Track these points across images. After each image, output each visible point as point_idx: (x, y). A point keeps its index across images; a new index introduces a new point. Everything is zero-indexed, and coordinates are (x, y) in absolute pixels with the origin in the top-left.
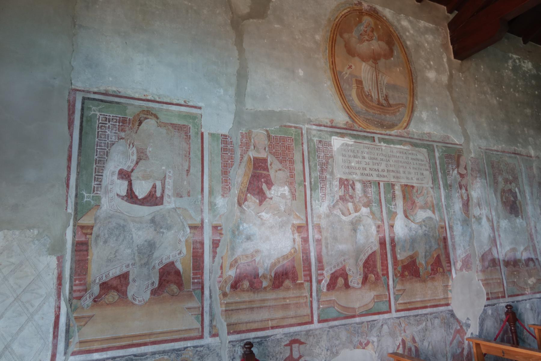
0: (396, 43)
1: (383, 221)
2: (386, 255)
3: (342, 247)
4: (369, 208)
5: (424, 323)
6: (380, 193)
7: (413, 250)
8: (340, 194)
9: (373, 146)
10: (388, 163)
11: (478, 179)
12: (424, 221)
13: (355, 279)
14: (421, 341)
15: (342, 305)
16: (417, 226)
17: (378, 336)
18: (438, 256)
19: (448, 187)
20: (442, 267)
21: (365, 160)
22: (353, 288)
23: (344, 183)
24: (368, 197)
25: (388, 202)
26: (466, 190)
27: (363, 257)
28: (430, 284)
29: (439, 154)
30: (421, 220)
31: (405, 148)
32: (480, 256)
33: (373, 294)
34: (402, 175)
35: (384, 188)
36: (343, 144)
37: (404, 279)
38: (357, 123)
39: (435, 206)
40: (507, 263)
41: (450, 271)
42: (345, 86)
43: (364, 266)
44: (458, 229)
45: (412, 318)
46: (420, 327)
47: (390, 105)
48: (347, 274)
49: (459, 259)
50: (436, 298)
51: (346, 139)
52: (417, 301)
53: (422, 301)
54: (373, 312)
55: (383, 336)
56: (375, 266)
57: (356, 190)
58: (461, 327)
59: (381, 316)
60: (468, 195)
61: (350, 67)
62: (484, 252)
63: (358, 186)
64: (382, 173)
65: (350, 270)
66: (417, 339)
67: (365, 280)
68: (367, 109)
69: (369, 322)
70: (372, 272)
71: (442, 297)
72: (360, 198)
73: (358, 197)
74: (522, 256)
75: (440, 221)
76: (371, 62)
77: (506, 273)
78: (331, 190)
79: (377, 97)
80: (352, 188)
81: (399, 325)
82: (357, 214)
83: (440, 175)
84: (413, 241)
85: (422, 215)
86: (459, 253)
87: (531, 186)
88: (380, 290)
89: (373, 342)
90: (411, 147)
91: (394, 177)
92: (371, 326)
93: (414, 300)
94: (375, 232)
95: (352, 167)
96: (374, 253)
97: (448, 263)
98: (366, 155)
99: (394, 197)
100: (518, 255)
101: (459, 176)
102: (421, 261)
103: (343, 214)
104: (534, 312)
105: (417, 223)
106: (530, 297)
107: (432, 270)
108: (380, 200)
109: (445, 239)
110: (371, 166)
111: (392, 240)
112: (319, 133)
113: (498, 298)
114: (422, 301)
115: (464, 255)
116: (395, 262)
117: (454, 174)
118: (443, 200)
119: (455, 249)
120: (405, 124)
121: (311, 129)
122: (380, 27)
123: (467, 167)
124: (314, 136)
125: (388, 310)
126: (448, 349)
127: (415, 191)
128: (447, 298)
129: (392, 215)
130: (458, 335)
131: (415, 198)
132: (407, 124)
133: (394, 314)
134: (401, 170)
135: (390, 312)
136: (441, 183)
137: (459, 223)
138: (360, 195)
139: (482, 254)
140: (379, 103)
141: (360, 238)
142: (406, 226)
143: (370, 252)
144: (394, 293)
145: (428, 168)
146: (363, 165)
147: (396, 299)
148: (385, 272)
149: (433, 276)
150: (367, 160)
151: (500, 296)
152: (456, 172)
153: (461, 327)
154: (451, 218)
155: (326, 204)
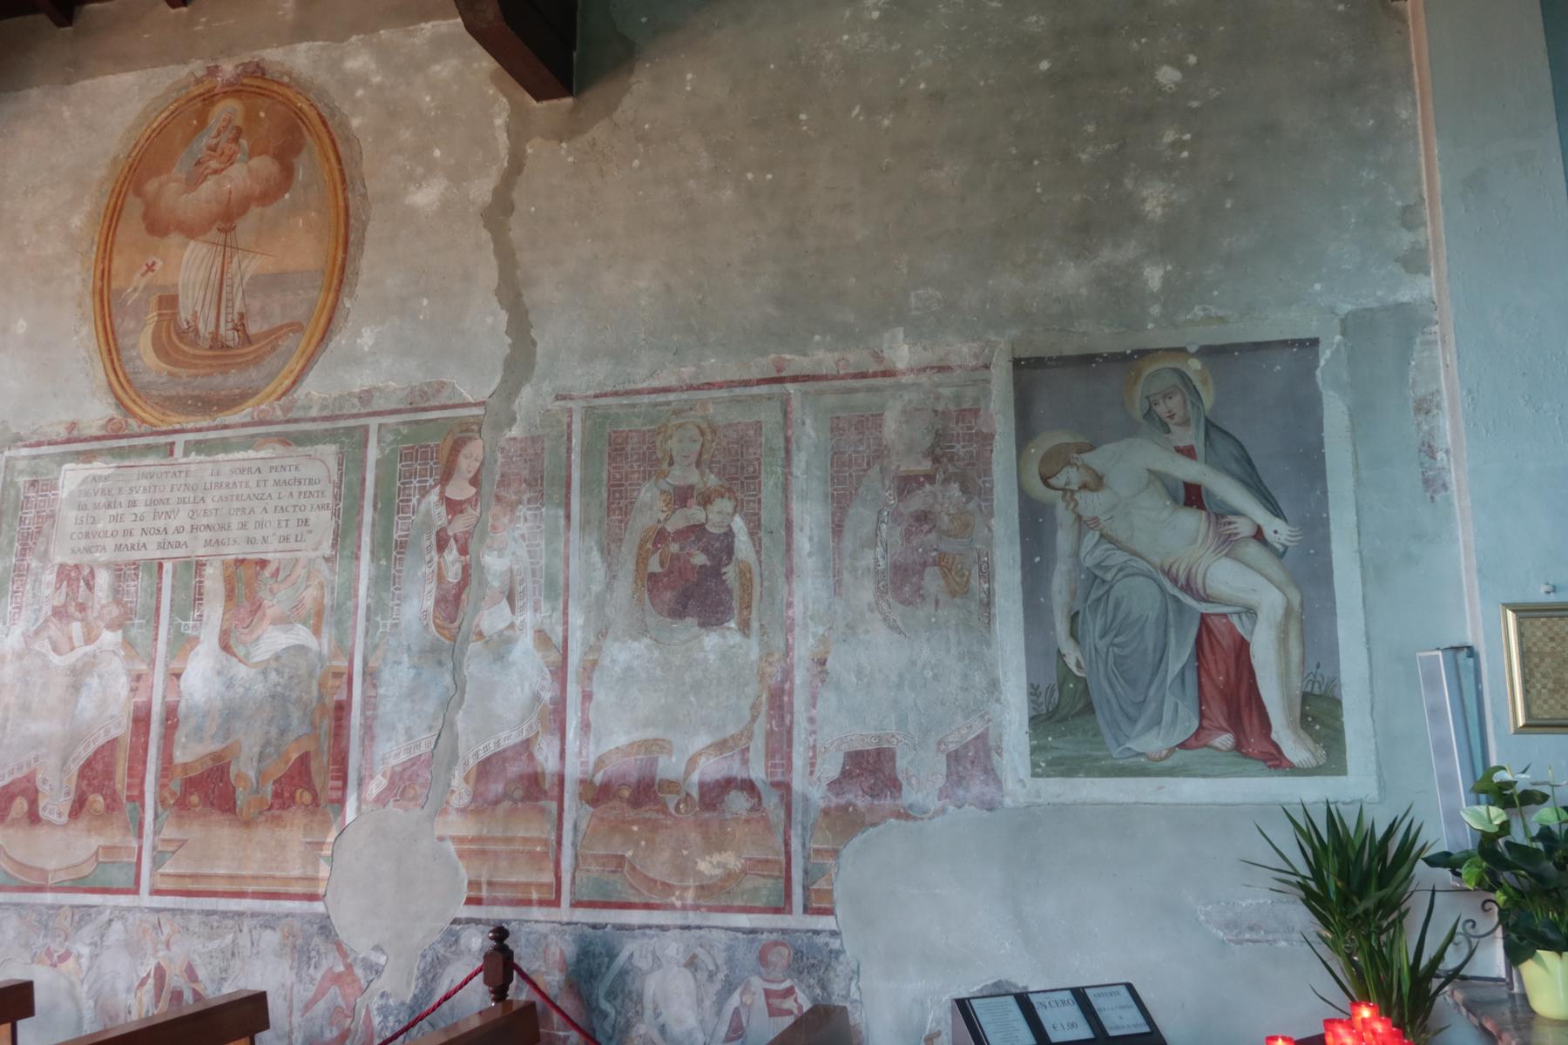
0: (309, 140)
1: (153, 662)
2: (146, 750)
3: (37, 727)
4: (120, 632)
5: (231, 936)
6: (160, 590)
7: (226, 738)
8: (56, 603)
9: (164, 469)
10: (201, 506)
11: (522, 511)
12: (277, 657)
13: (55, 804)
14: (212, 981)
15: (18, 858)
16: (253, 672)
17: (95, 944)
18: (304, 759)
19: (390, 549)
20: (310, 787)
21: (135, 510)
22: (50, 823)
23: (68, 575)
24: (124, 605)
25: (179, 611)
26: (463, 551)
27: (83, 753)
28: (262, 833)
29: (382, 450)
30: (267, 656)
31: (262, 454)
32: (472, 762)
33: (96, 842)
34: (236, 533)
35: (174, 576)
36: (84, 481)
37: (185, 813)
38: (134, 415)
39: (327, 612)
40: (598, 793)
41: (341, 802)
42: (126, 324)
43: (82, 774)
44: (398, 676)
45: (247, 923)
46: (214, 944)
47: (247, 340)
48: (37, 791)
49: (380, 768)
50: (278, 874)
51: (96, 464)
52: (216, 876)
53: (231, 878)
54: (89, 884)
55: (108, 948)
56: (109, 775)
57: (96, 589)
58: (349, 967)
59: (108, 897)
60: (466, 569)
61: (150, 268)
62: (492, 749)
63: (103, 579)
64: (172, 538)
65: (44, 781)
66: (201, 973)
67: (78, 807)
68: (175, 370)
69: (78, 907)
70: (98, 790)
71: (296, 873)
72: (103, 607)
73: (97, 607)
74: (688, 773)
75: (334, 656)
76: (213, 234)
77: (583, 826)
78: (34, 596)
79: (212, 328)
80: (87, 584)
81: (154, 928)
82: (89, 648)
83: (368, 515)
84: (231, 714)
85: (273, 640)
86: (385, 751)
87: (840, 503)
88: (114, 836)
89: (79, 956)
90: (280, 449)
91: (208, 543)
92: (81, 919)
93: (205, 871)
94: (124, 692)
95: (97, 534)
96: (113, 743)
97: (337, 778)
98: (141, 497)
99: (199, 597)
100: (669, 766)
101: (443, 509)
102: (245, 768)
103: (56, 649)
104: (702, 976)
105: (255, 665)
106: (693, 918)
107: (276, 795)
108: (158, 609)
109: (342, 709)
110: (149, 523)
111: (171, 714)
112: (33, 462)
113: (528, 903)
114: (231, 877)
115: (403, 757)
116: (165, 769)
117: (422, 508)
118: (362, 591)
119: (372, 738)
120: (287, 382)
121: (15, 459)
122: (262, 114)
123: (483, 476)
124: (21, 472)
125: (131, 885)
126: (297, 1019)
127: (267, 572)
128: (313, 880)
129: (183, 644)
130: (334, 990)
131: (263, 593)
132: (294, 383)
133: (145, 899)
134: (235, 521)
135: (135, 890)
136: (366, 539)
137: (405, 658)
138: (104, 602)
139: (482, 755)
140: (217, 343)
141: (87, 704)
142: (219, 673)
143: (102, 741)
144: (154, 848)
145: (329, 500)
146: (128, 524)
147: (157, 862)
148: (136, 793)
149: (277, 813)
150: (140, 509)
151: (535, 896)
152: (433, 497)
153: (349, 967)
154: (376, 647)
155: (17, 631)
